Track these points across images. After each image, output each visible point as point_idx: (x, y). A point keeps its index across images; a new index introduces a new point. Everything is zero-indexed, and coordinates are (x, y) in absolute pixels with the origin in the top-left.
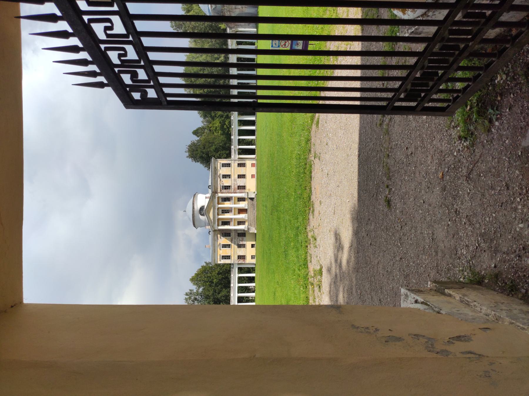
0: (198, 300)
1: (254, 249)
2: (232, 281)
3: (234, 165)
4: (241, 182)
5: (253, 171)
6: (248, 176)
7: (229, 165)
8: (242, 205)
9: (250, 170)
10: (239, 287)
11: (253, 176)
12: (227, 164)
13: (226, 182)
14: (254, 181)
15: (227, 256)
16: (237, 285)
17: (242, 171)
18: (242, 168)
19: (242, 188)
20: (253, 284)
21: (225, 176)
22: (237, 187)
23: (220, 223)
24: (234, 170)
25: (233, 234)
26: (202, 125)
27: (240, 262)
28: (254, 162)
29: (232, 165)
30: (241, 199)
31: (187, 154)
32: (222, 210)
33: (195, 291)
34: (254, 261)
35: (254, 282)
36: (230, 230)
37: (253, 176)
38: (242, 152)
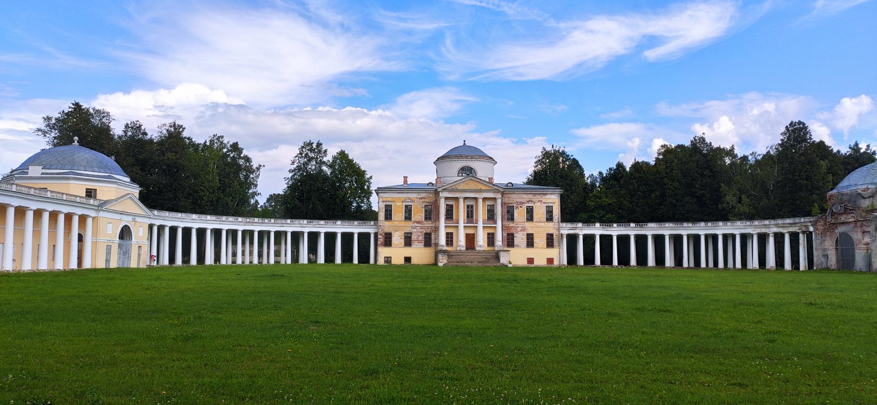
0: (307, 164)
1: (402, 262)
2: (346, 223)
3: (550, 228)
4: (520, 239)
5: (540, 261)
6: (530, 253)
7: (550, 218)
8: (481, 241)
9: (541, 255)
10: (610, 237)
11: (531, 261)
12: (552, 216)
13: (520, 214)
14: (523, 262)
15: (391, 214)
16: (306, 230)
17: (540, 241)
18: (536, 240)
19: (510, 241)
20: (356, 260)
21: (530, 212)
22: (530, 232)
23: (450, 203)
24: (541, 228)
25: (429, 224)
26: (587, 176)
27: (380, 236)
28: (556, 263)
29: (550, 224)
30: (491, 239)
31: (549, 148)
32: (472, 206)
33: (325, 159)
34: (381, 261)
35: (359, 262)
36: (438, 219)
37: (531, 261)
38: (572, 240)
